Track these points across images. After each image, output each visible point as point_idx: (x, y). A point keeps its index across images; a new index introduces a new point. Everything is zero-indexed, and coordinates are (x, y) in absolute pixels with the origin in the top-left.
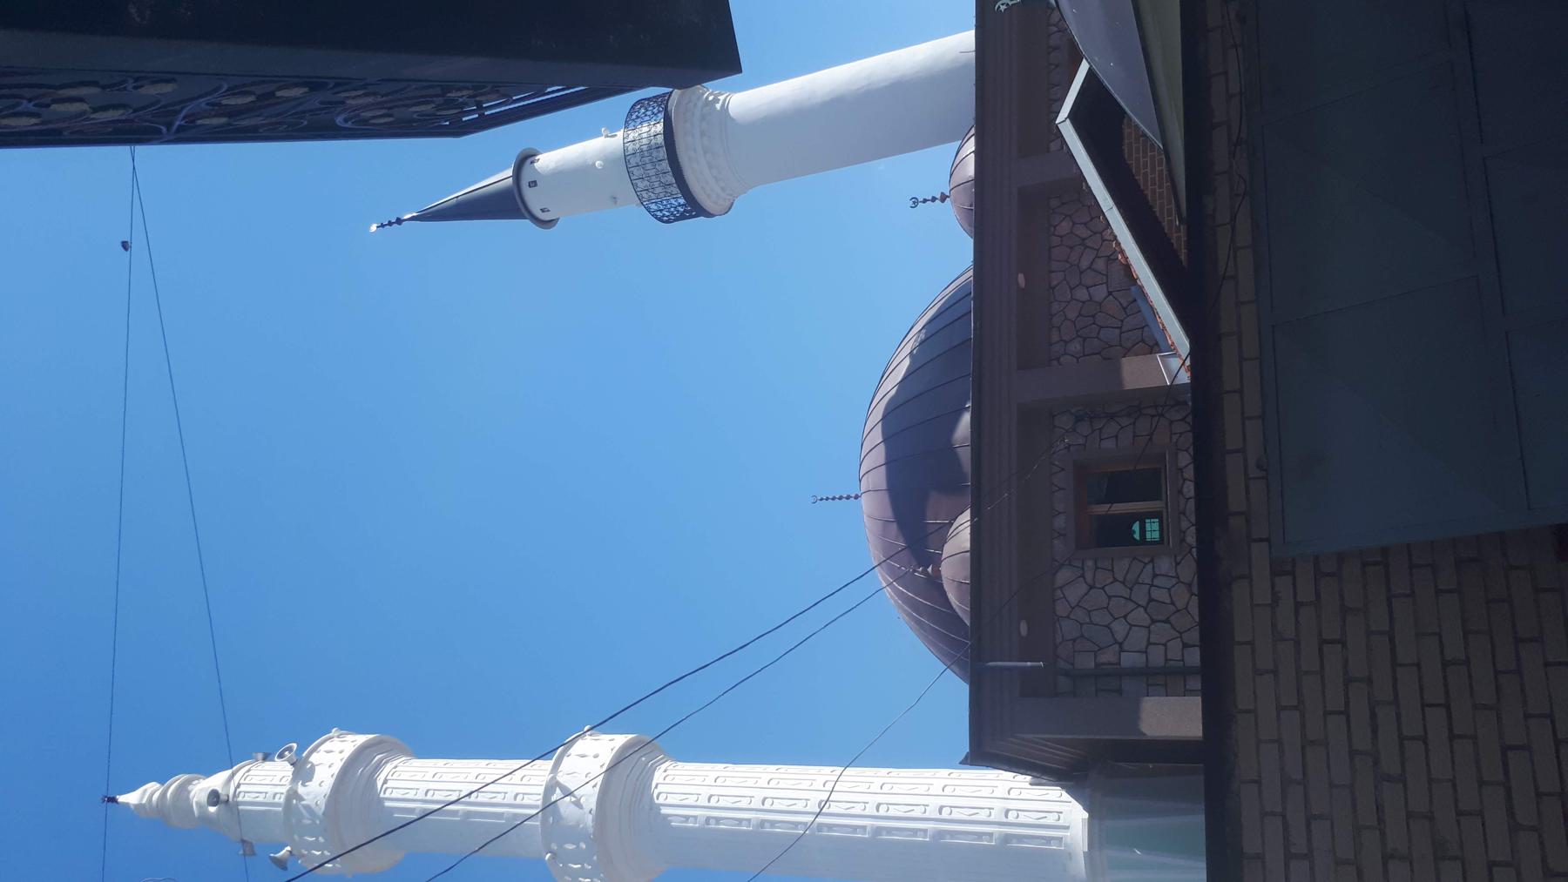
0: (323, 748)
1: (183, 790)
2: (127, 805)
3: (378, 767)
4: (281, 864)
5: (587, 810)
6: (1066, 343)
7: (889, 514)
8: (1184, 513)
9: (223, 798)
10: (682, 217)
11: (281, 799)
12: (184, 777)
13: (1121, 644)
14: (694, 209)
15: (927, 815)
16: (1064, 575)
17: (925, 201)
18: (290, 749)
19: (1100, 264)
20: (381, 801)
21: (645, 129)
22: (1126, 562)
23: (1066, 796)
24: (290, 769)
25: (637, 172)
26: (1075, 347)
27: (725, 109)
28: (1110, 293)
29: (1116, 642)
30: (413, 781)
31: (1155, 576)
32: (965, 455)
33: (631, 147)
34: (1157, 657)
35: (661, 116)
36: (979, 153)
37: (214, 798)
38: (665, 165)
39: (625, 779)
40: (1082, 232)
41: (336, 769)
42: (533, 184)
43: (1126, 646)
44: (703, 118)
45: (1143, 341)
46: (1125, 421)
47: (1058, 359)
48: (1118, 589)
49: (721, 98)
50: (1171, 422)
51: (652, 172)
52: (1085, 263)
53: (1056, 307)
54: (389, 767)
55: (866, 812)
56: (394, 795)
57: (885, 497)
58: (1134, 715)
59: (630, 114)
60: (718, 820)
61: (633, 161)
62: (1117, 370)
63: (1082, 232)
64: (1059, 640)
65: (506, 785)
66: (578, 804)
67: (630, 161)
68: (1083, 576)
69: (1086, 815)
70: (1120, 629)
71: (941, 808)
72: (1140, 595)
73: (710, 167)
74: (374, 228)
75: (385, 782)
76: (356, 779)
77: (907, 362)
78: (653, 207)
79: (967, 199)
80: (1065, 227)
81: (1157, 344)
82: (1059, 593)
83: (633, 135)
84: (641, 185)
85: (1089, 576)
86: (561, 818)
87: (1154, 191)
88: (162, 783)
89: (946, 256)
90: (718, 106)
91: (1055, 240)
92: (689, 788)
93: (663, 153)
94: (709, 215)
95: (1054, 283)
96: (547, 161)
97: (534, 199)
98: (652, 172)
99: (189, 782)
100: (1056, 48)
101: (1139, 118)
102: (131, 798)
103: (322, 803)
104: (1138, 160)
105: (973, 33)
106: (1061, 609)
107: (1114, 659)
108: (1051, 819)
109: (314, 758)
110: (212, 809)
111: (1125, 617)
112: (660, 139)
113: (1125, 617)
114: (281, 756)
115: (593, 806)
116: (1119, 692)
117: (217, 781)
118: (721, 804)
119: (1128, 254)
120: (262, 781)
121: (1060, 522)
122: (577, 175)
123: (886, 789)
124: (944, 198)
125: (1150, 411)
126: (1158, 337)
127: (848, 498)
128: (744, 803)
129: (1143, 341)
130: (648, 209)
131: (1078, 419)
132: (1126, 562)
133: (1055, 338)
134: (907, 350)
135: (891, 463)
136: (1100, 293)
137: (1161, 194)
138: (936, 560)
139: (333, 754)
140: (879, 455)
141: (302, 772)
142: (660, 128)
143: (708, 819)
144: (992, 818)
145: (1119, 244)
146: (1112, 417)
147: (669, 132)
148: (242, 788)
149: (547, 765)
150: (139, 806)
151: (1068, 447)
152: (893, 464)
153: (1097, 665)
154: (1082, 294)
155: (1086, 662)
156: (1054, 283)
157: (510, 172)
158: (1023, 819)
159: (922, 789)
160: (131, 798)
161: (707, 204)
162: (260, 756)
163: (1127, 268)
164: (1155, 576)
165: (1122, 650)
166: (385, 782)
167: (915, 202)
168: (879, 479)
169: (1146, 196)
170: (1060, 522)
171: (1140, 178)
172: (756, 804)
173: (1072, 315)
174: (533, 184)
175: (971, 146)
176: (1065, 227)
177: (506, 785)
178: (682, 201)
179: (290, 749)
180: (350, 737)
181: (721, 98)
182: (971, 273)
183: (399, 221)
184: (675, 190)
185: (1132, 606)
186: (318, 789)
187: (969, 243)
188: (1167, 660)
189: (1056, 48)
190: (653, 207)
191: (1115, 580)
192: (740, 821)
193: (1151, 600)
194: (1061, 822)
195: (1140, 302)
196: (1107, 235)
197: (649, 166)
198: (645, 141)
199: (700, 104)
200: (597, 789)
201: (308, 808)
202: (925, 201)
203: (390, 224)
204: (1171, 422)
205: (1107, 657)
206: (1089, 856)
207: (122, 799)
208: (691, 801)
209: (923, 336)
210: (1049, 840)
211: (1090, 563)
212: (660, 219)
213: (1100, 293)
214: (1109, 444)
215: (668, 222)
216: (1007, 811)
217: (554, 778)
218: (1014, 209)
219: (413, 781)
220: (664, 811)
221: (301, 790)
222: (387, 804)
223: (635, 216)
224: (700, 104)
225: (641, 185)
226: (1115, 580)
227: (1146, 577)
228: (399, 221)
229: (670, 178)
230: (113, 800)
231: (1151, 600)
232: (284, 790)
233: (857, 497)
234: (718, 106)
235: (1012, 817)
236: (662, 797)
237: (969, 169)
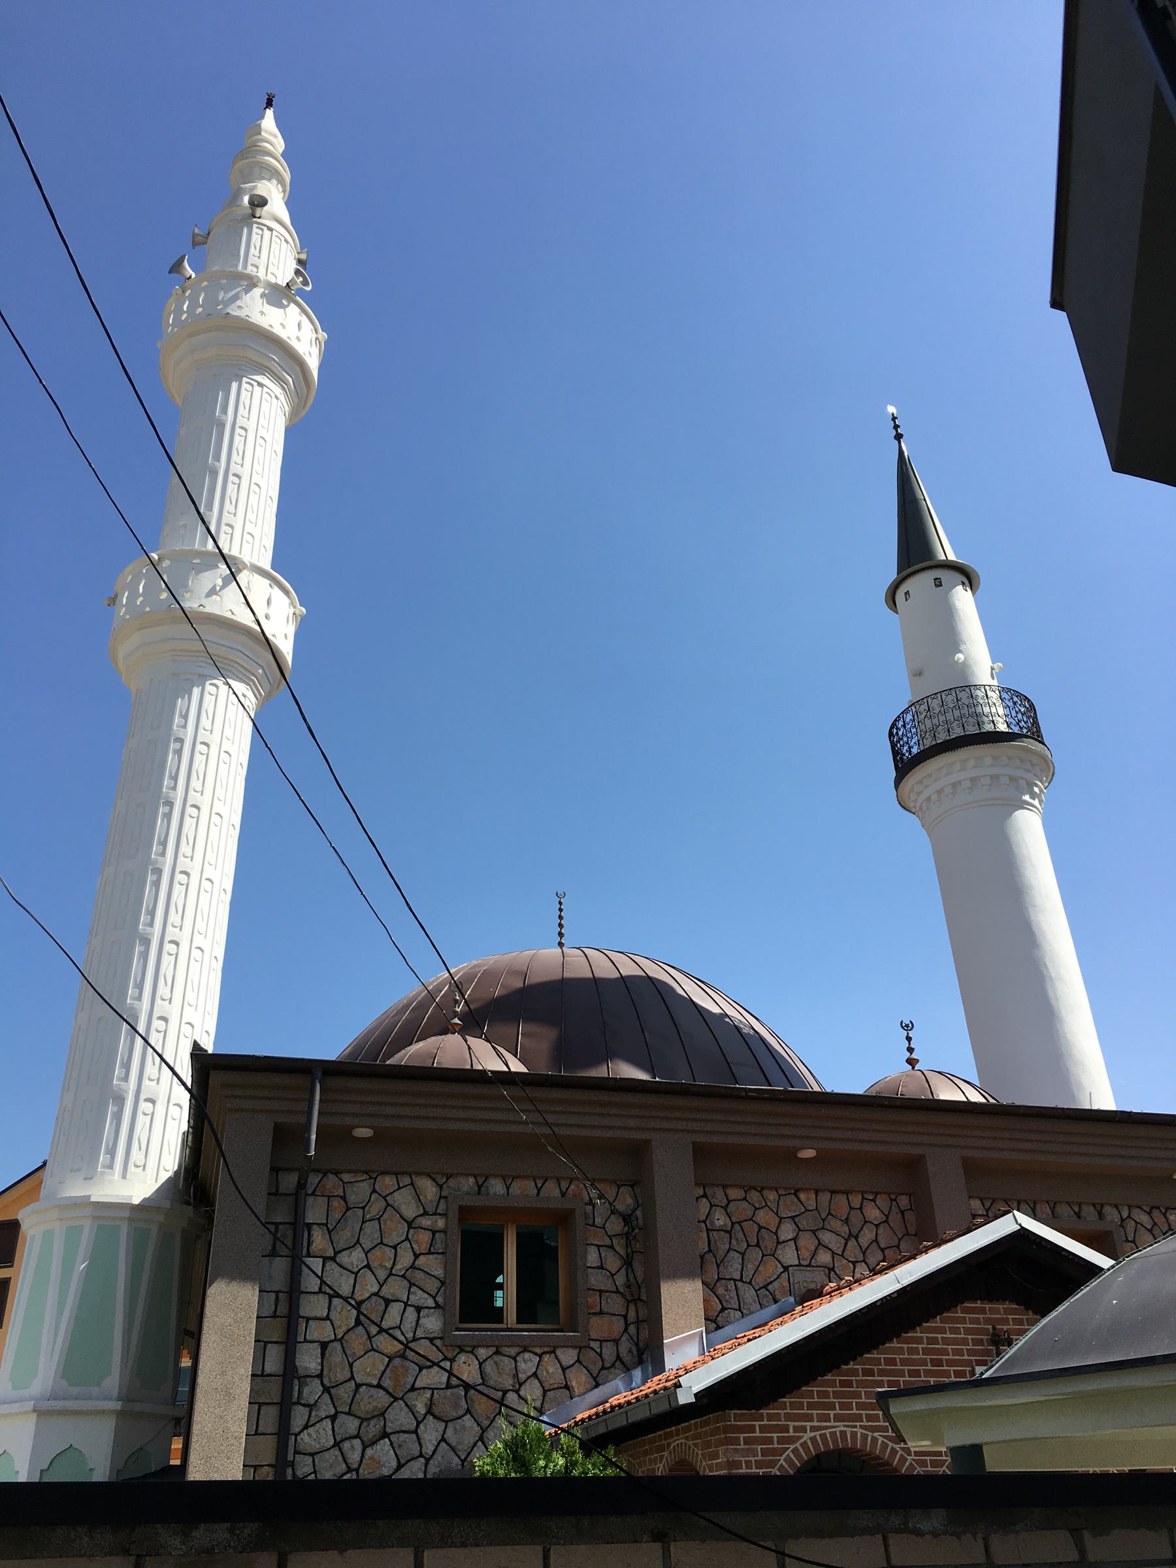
0: (304, 319)
1: (274, 174)
2: (262, 117)
3: (279, 380)
4: (177, 267)
5: (205, 602)
6: (725, 1208)
7: (535, 978)
8: (497, 1353)
9: (258, 212)
10: (896, 753)
11: (250, 270)
12: (287, 177)
13: (333, 1259)
14: (904, 766)
15: (158, 1001)
16: (429, 1189)
17: (909, 1039)
18: (305, 283)
19: (824, 1257)
20: (239, 379)
21: (1001, 711)
22: (439, 1272)
23: (165, 1176)
24: (283, 282)
25: (950, 699)
26: (720, 1219)
27: (1023, 805)
28: (786, 1268)
29: (336, 1253)
30: (259, 420)
31: (419, 1309)
32: (600, 1072)
33: (980, 693)
34: (313, 1306)
35: (1016, 730)
36: (966, 1108)
37: (259, 202)
38: (957, 732)
39: (234, 649)
40: (867, 1236)
41: (282, 334)
42: (938, 583)
43: (330, 1265)
44: (1013, 779)
45: (723, 1309)
46: (620, 1279)
47: (705, 1196)
48: (406, 1259)
49: (1036, 802)
50: (616, 1342)
51: (950, 716)
52: (826, 1237)
53: (772, 1196)
54: (277, 390)
55: (169, 928)
56: (243, 393)
57: (555, 975)
58: (239, 1274)
59: (1019, 695)
60: (179, 752)
61: (963, 696)
62: (688, 1275)
63: (867, 1236)
64: (346, 1177)
65: (249, 515)
66: (213, 592)
67: (963, 691)
68: (425, 1213)
69: (136, 1201)
70: (355, 1258)
71: (165, 1019)
72: (397, 1288)
73: (954, 785)
74: (891, 409)
75: (260, 385)
76: (273, 354)
77: (716, 1010)
78: (909, 717)
79: (912, 1090)
80: (873, 1213)
81: (718, 1328)
82: (407, 1180)
83: (994, 696)
84: (935, 704)
85: (426, 1222)
86: (198, 572)
87: (919, 1341)
88: (283, 155)
89: (841, 1056)
90: (1027, 798)
91: (856, 1200)
92: (221, 726)
93: (972, 730)
94: (898, 782)
95: (802, 1196)
96: (963, 599)
97: (920, 584)
98: (950, 716)
99: (281, 181)
100: (1100, 1214)
101: (1037, 1338)
102: (269, 121)
103: (242, 314)
104: (963, 1320)
105: (1111, 1106)
106: (388, 1182)
107: (314, 1248)
108: (137, 1156)
109: (293, 308)
110: (246, 199)
111: (368, 1266)
112: (989, 727)
113: (368, 1266)
114: (297, 272)
115: (208, 610)
116: (273, 1254)
117: (277, 205)
118: (197, 756)
119: (837, 1301)
120: (274, 253)
121: (497, 1187)
122: (951, 638)
123: (196, 953)
124: (912, 1062)
125: (632, 1315)
126: (727, 1330)
127: (561, 935)
128: (195, 783)
129: (723, 1309)
130: (905, 712)
131: (627, 1219)
132: (439, 1272)
133: (734, 1193)
134: (730, 1012)
135: (596, 983)
136: (789, 1255)
137: (916, 1351)
138: (464, 1031)
139: (298, 330)
140: (605, 970)
141: (279, 295)
142: (1002, 727)
143: (181, 741)
144: (146, 1082)
145: (849, 1285)
146: (628, 1263)
147: (996, 737)
148: (267, 233)
149: (266, 565)
150: (258, 130)
151: (591, 1203)
152: (594, 988)
153: (309, 1226)
154: (787, 1231)
155: (315, 1212)
156: (802, 1196)
157: (952, 557)
158: (142, 1121)
159: (191, 997)
160: (269, 121)
161: (912, 779)
162: (303, 257)
163: (812, 1294)
164: (419, 1309)
165: (325, 1259)
166: (260, 385)
167: (907, 1027)
168: (578, 969)
169: (912, 1328)
170: (497, 1187)
171: (937, 1323)
172: (193, 797)
173: (763, 1217)
174: (938, 583)
175: (975, 1097)
176: (873, 1213)
177: (249, 515)
178: (915, 750)
179: (305, 283)
180: (315, 351)
181: (1036, 802)
182: (817, 1089)
183: (899, 437)
184: (928, 742)
185: (382, 1274)
186: (256, 309)
187: (857, 1087)
188: (308, 1319)
189: (1100, 1214)
190: (909, 717)
191: (416, 1256)
192: (175, 778)
193: (388, 1302)
194: (131, 1168)
195: (774, 1307)
196: (862, 1269)
197: (957, 713)
198: (986, 710)
199: (1029, 776)
200: (228, 615)
201: (237, 297)
202: (909, 1039)
203: (896, 427)
204: (616, 1342)
205: (319, 1241)
206: (84, 1203)
207: (269, 113)
208: (205, 722)
209: (746, 1030)
210: (112, 1152)
211: (441, 1223)
212: (893, 725)
213: (789, 1255)
214: (592, 1257)
215: (891, 734)
216: (153, 1102)
217: (245, 566)
218: (899, 1152)
219: (259, 420)
220: (196, 691)
221: (257, 292)
222: (234, 385)
223: (898, 696)
224: (1029, 776)
225: (935, 704)
226: (416, 1256)
227: (418, 1297)
228: (899, 437)
229: (942, 737)
230: (269, 104)
231: (388, 1302)
232: (261, 274)
233: (561, 945)
234: (1027, 798)
235: (144, 1106)
236: (213, 690)
237: (947, 1093)
